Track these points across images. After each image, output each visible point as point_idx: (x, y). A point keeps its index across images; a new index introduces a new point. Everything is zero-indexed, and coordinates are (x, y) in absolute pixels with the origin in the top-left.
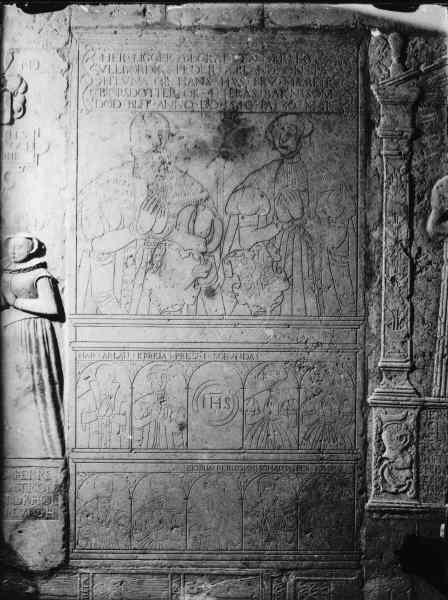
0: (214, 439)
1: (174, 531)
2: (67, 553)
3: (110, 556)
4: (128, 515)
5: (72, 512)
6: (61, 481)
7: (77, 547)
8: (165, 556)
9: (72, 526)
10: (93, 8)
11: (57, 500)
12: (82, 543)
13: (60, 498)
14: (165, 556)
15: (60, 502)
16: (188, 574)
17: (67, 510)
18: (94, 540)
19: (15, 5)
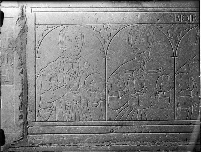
0: (137, 3)
1: (159, 96)
2: (25, 124)
3: (80, 128)
4: (102, 77)
5: (30, 75)
6: (16, 35)
7: (38, 118)
8: (147, 127)
9: (31, 92)
10: (6, 142)
11: (12, 59)
12: (44, 113)
13: (16, 56)
14: (147, 127)
15: (16, 62)
16: (79, 121)
17: (24, 72)
18: (58, 110)
19: (1, 28)
